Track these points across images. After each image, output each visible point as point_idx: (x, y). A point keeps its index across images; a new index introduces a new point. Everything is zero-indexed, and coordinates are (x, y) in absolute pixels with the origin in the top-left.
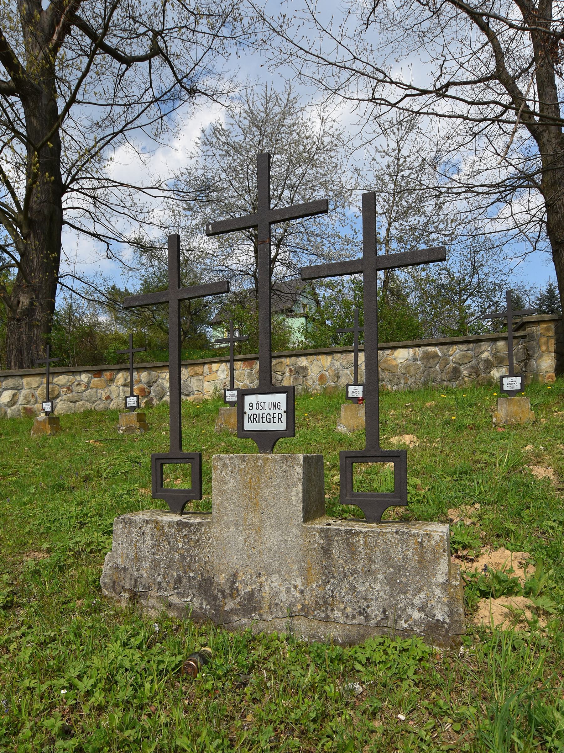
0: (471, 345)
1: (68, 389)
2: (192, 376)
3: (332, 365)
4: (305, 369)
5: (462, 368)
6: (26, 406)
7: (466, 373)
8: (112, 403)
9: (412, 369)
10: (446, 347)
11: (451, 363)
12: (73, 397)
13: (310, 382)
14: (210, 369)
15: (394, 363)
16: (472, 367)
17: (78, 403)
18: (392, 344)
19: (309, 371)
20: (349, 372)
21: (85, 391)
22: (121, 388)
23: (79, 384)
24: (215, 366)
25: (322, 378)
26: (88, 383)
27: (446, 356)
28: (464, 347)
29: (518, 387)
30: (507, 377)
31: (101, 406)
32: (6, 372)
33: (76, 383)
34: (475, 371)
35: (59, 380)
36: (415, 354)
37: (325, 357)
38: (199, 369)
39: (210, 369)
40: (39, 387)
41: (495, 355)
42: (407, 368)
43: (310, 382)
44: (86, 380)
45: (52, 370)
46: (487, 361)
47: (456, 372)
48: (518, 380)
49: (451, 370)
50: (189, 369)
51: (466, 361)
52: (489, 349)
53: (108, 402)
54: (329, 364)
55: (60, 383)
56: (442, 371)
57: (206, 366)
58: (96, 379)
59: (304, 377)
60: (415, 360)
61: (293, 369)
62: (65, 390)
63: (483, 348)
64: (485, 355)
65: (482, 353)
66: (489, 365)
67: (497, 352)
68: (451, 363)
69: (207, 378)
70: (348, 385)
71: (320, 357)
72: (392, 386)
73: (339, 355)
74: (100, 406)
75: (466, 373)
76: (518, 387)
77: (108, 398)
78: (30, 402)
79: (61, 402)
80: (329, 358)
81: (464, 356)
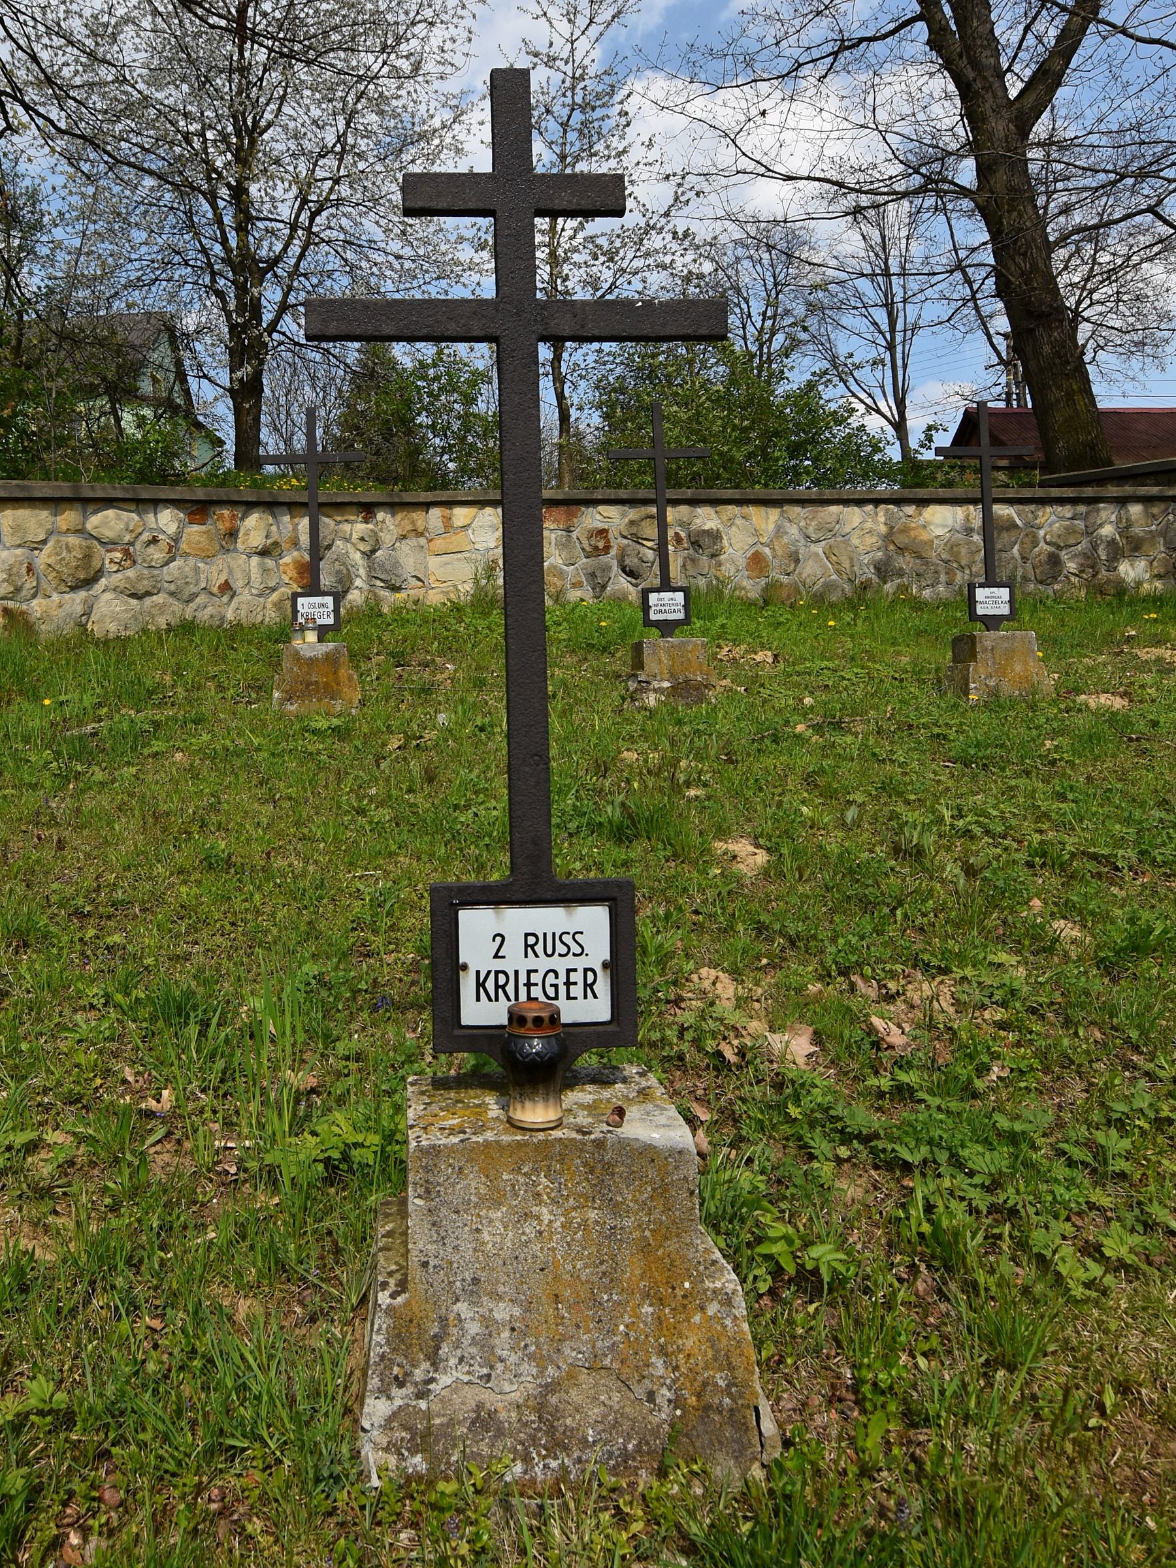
0: (1082, 509)
1: (126, 553)
2: (404, 537)
3: (779, 531)
4: (715, 536)
5: (1064, 555)
6: (10, 604)
7: (1072, 566)
8: (234, 604)
9: (963, 551)
10: (1033, 507)
11: (1042, 544)
12: (140, 578)
13: (728, 570)
14: (447, 521)
15: (925, 536)
16: (1085, 555)
17: (148, 601)
18: (922, 493)
19: (725, 542)
20: (820, 551)
21: (166, 564)
22: (255, 560)
23: (154, 541)
24: (461, 515)
25: (757, 562)
26: (176, 539)
27: (1032, 527)
28: (1067, 511)
29: (1005, 610)
30: (658, 590)
31: (209, 610)
32: (13, 487)
33: (146, 536)
34: (1090, 562)
35: (104, 523)
36: (967, 517)
37: (762, 510)
38: (418, 516)
39: (447, 521)
40: (44, 542)
41: (1125, 528)
42: (952, 547)
43: (728, 570)
44: (172, 529)
45: (328, 492)
46: (1112, 543)
47: (1054, 561)
48: (1004, 593)
49: (1043, 558)
50: (399, 516)
51: (1072, 541)
52: (1113, 518)
53: (225, 599)
54: (771, 527)
55: (108, 534)
56: (1025, 559)
57: (436, 513)
58: (196, 528)
59: (713, 556)
60: (969, 531)
61: (683, 535)
62: (118, 555)
63: (1103, 514)
64: (1107, 531)
65: (1101, 525)
66: (1116, 553)
67: (1129, 526)
68: (1042, 544)
69: (439, 544)
70: (295, 597)
71: (751, 510)
72: (921, 588)
73: (797, 509)
74: (205, 611)
75: (1072, 566)
76: (1005, 610)
77: (226, 587)
78: (18, 590)
79: (108, 596)
80: (774, 514)
81: (1070, 531)
